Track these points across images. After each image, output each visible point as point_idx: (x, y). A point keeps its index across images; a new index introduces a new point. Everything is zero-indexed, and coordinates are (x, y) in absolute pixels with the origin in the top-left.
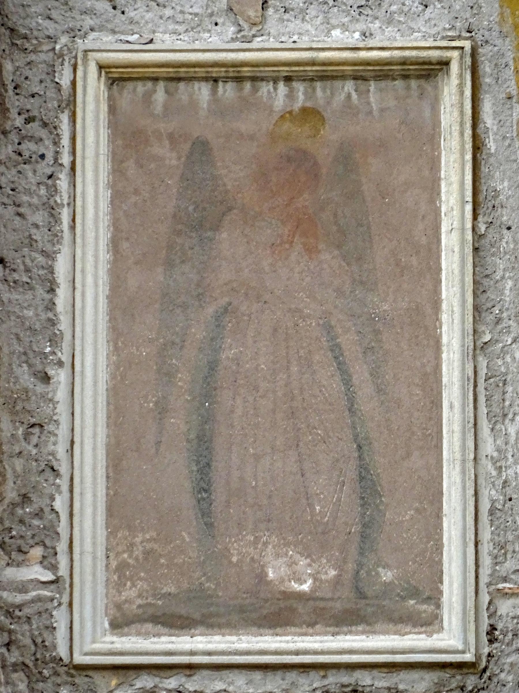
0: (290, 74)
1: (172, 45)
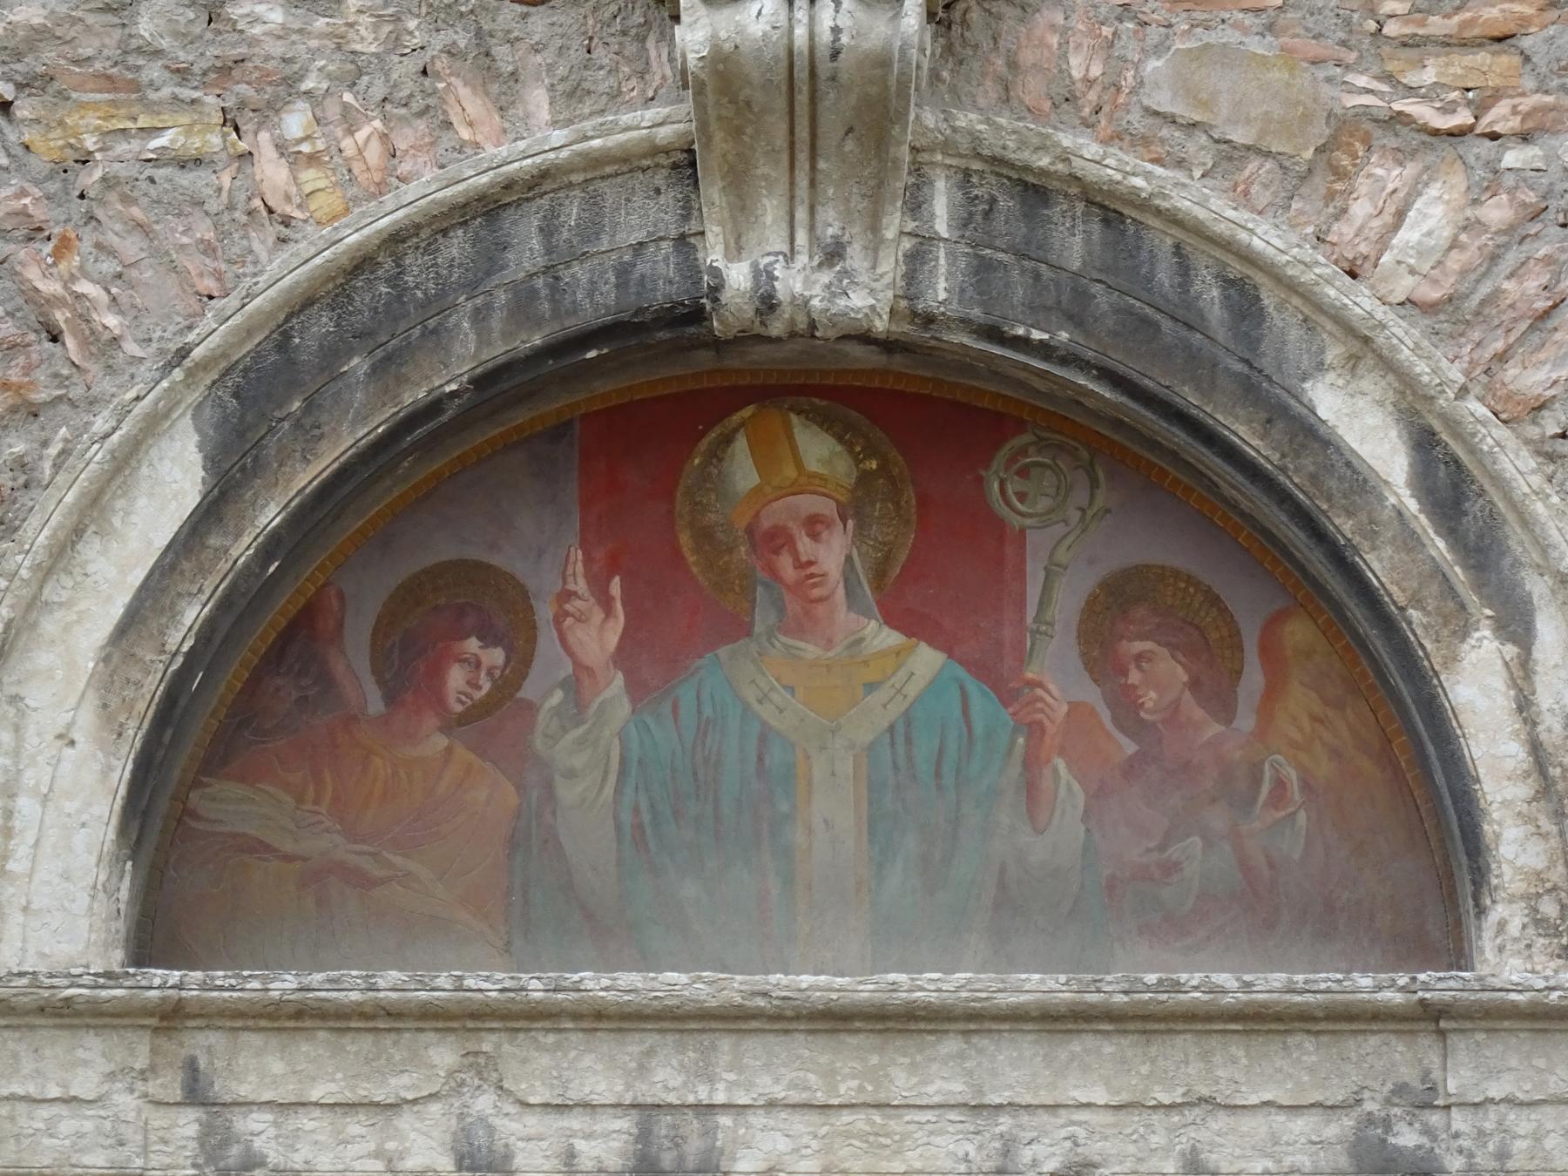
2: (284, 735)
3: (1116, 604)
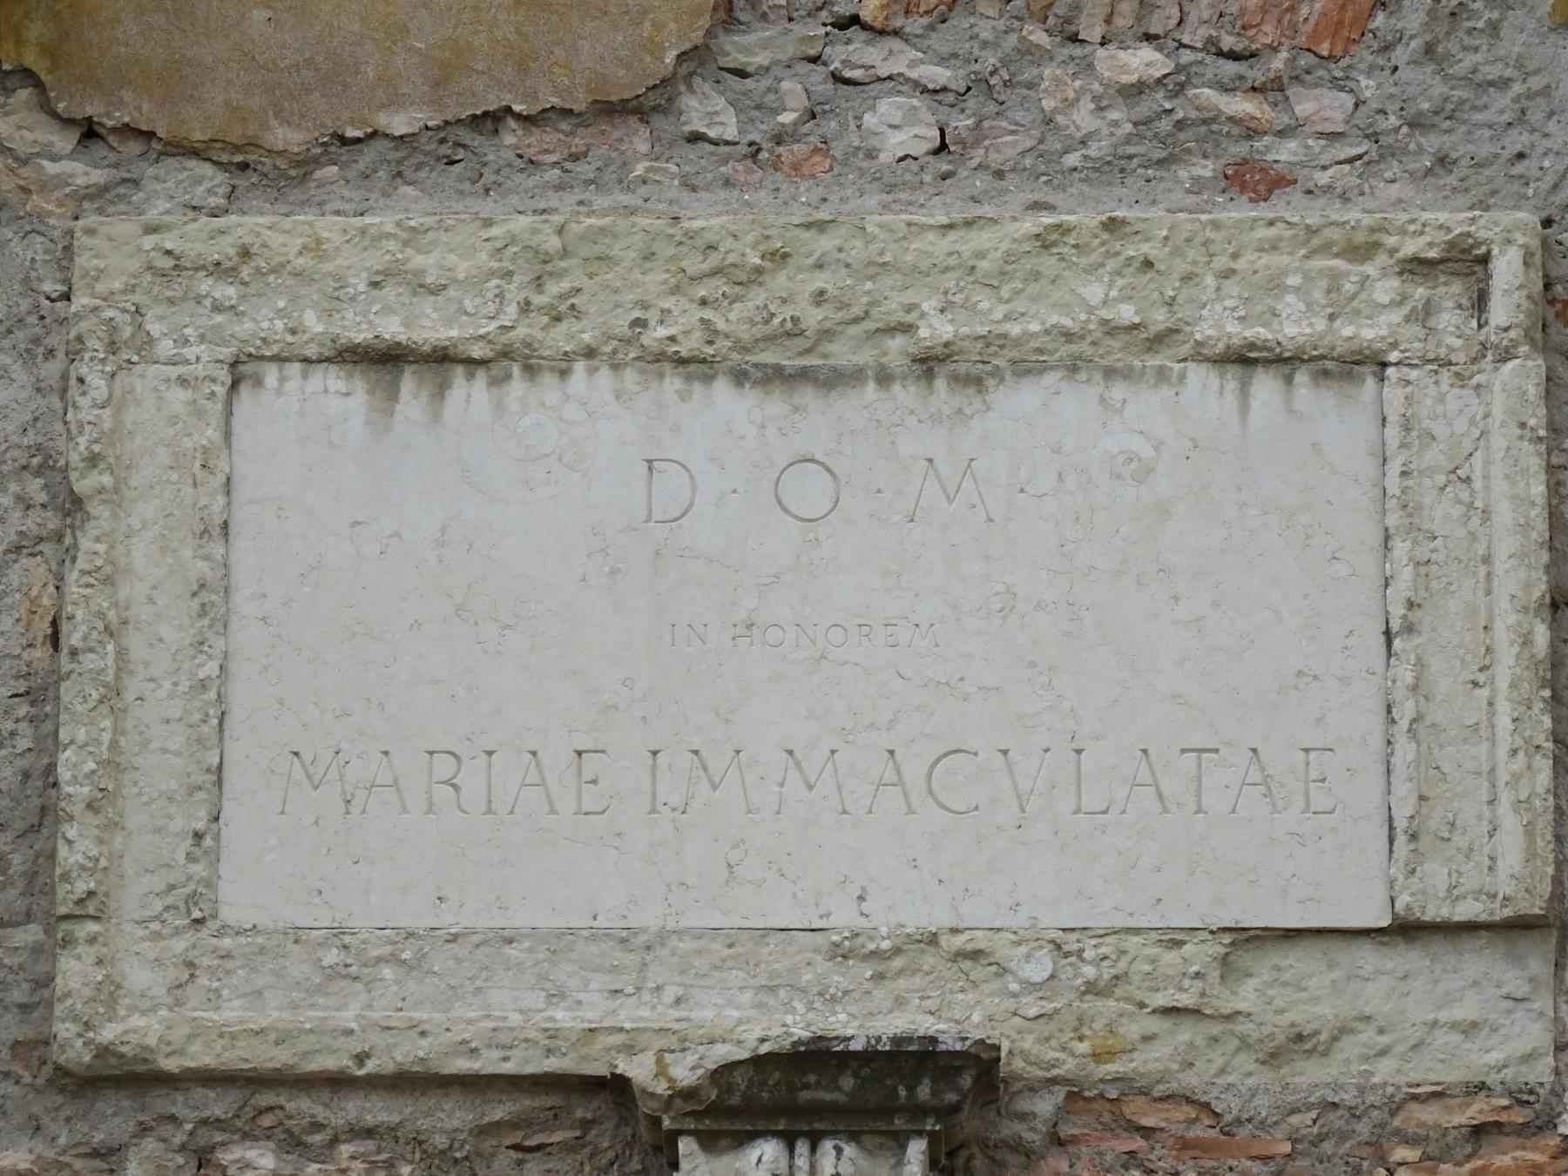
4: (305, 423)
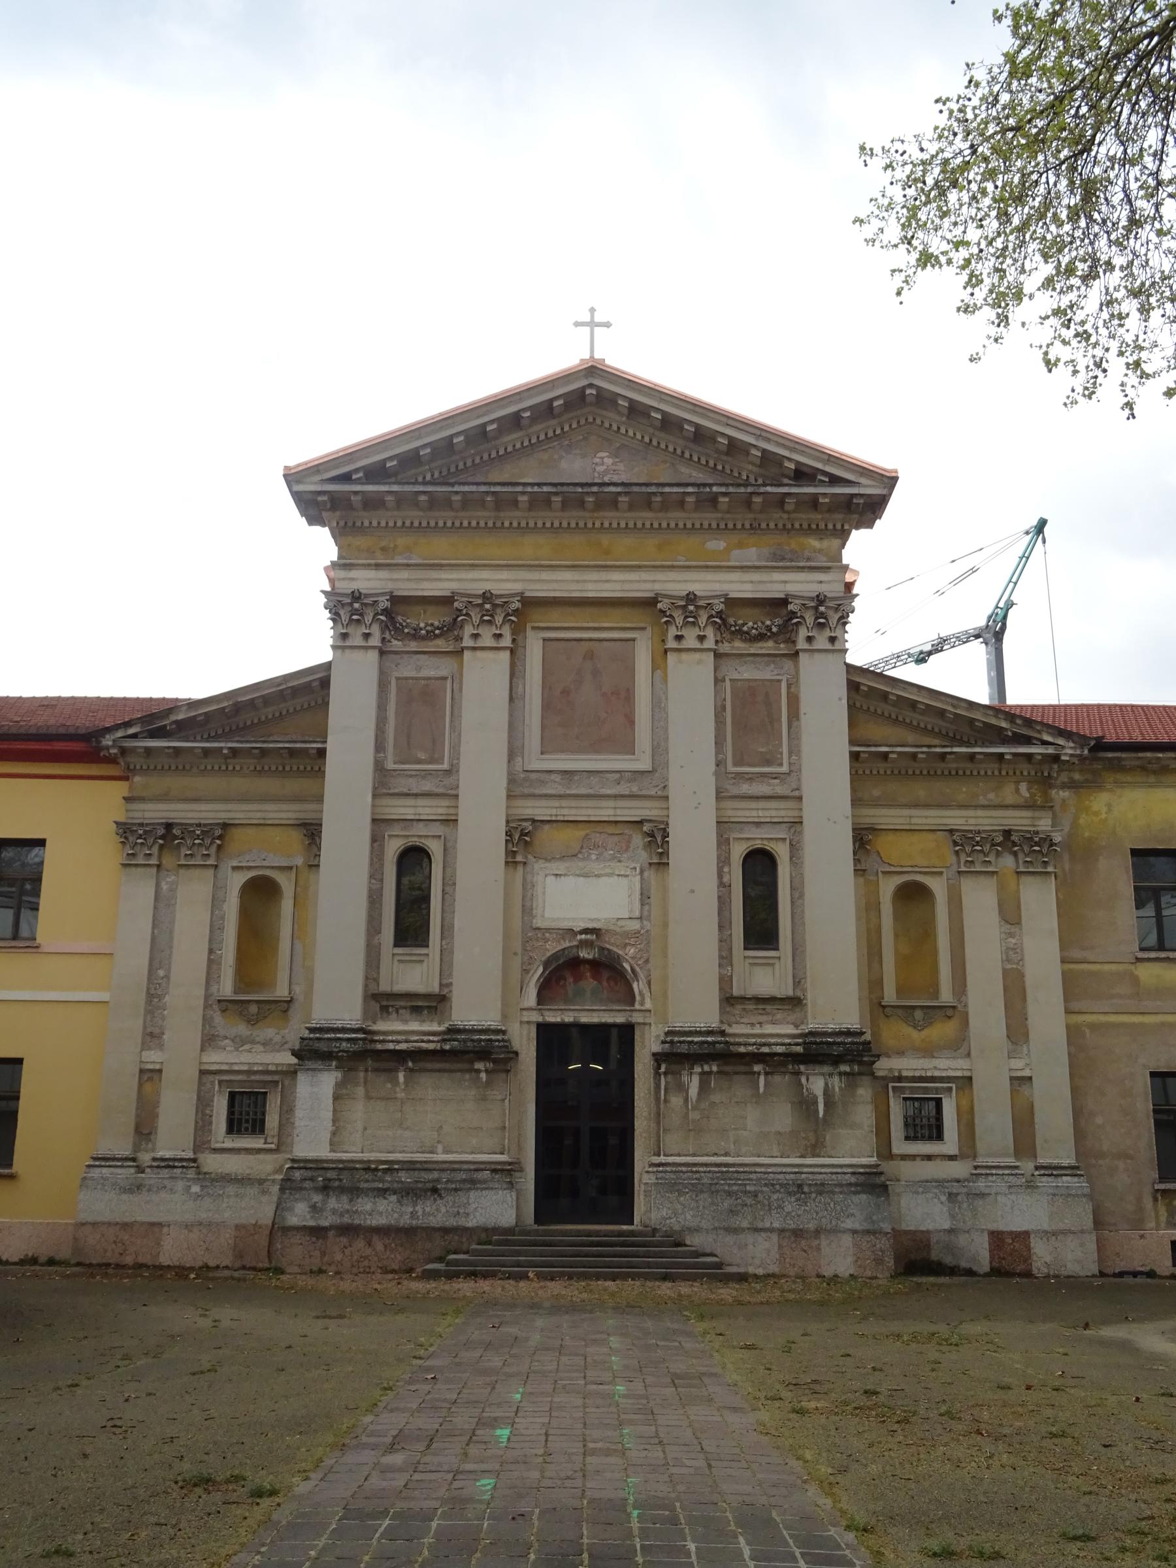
0: (424, 679)
1: (406, 674)
2: (854, 222)
3: (608, 979)
4: (550, 880)
